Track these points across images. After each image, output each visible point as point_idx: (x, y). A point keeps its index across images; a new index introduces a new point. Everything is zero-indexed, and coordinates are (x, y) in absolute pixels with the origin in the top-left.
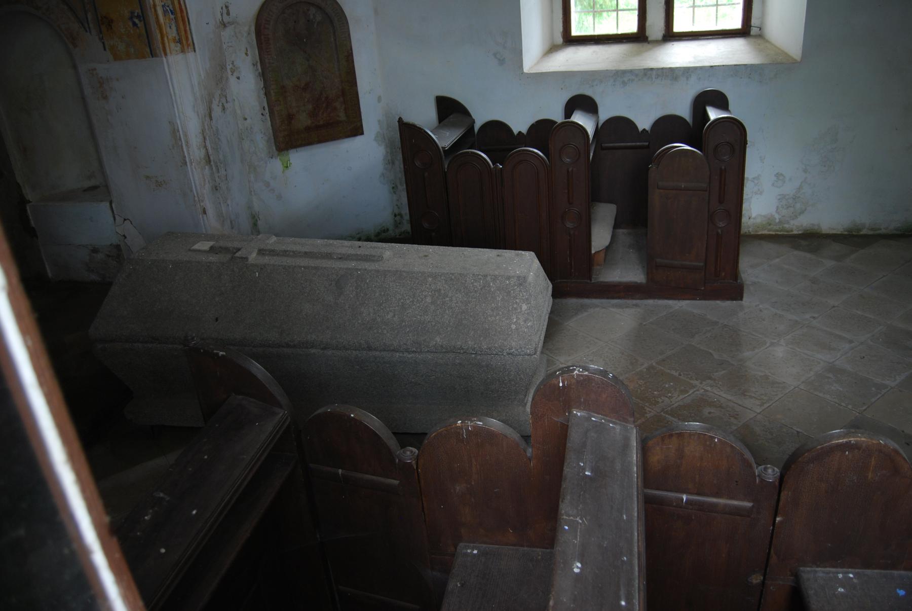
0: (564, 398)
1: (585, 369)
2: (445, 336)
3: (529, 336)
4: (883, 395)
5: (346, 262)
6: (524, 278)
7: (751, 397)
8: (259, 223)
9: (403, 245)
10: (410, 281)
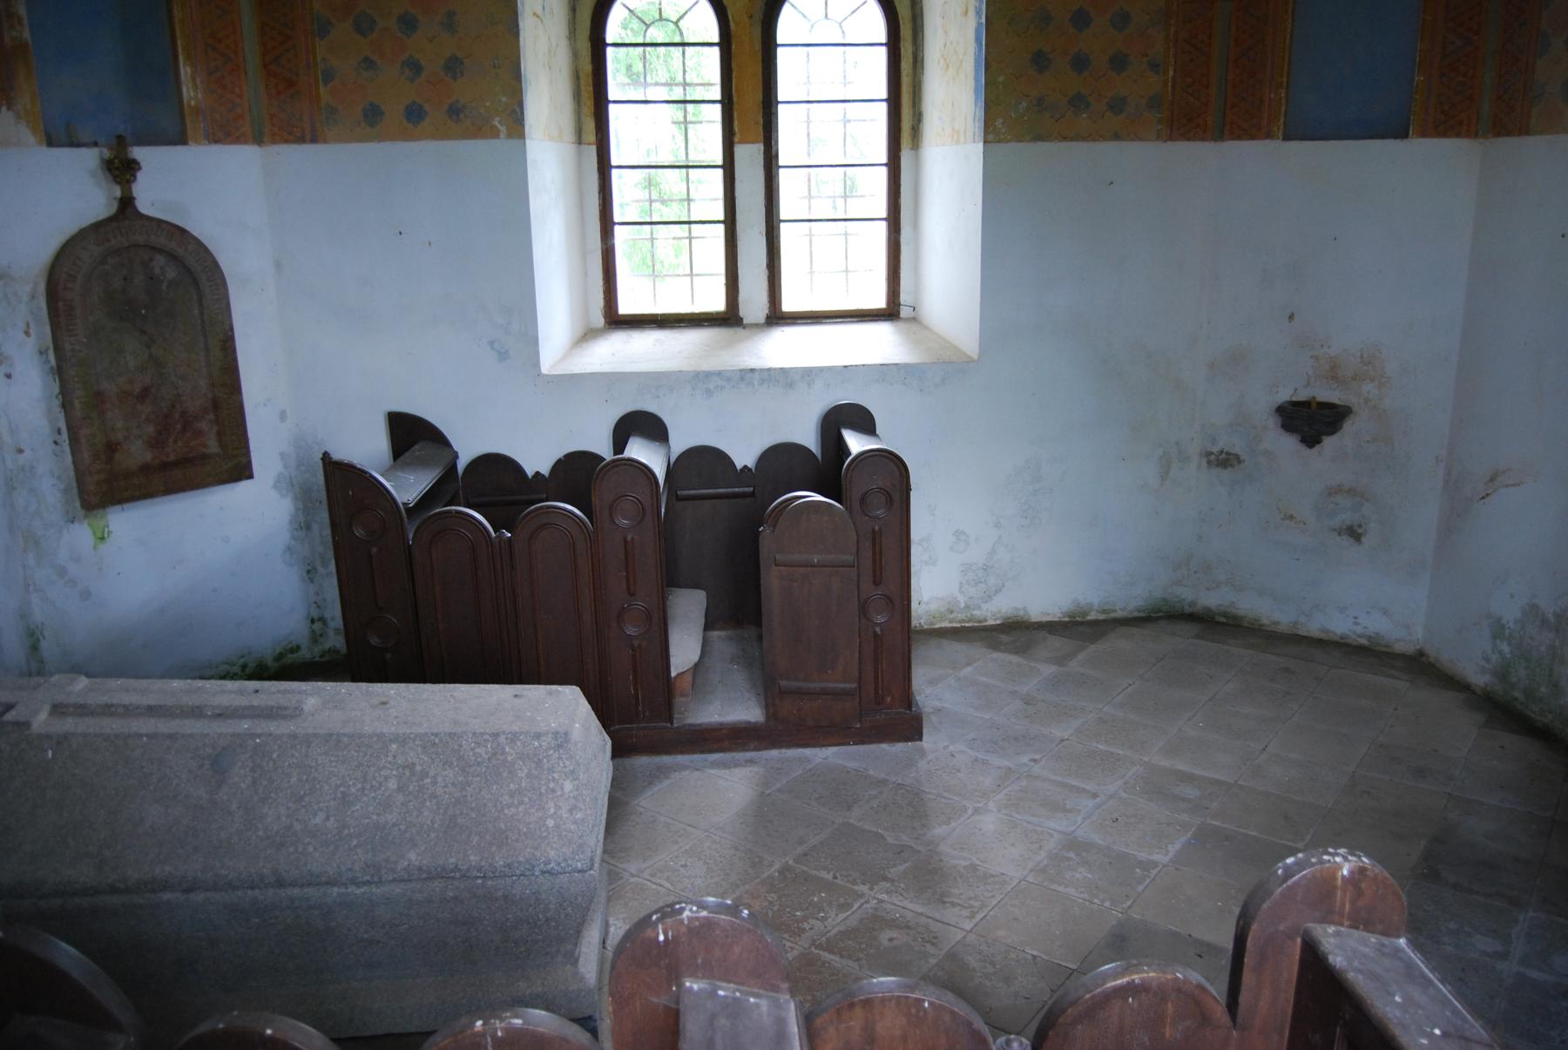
0: (667, 961)
1: (702, 906)
2: (426, 848)
3: (580, 837)
4: (1154, 879)
5: (231, 721)
6: (566, 734)
7: (954, 905)
8: (44, 644)
9: (339, 684)
10: (355, 751)
